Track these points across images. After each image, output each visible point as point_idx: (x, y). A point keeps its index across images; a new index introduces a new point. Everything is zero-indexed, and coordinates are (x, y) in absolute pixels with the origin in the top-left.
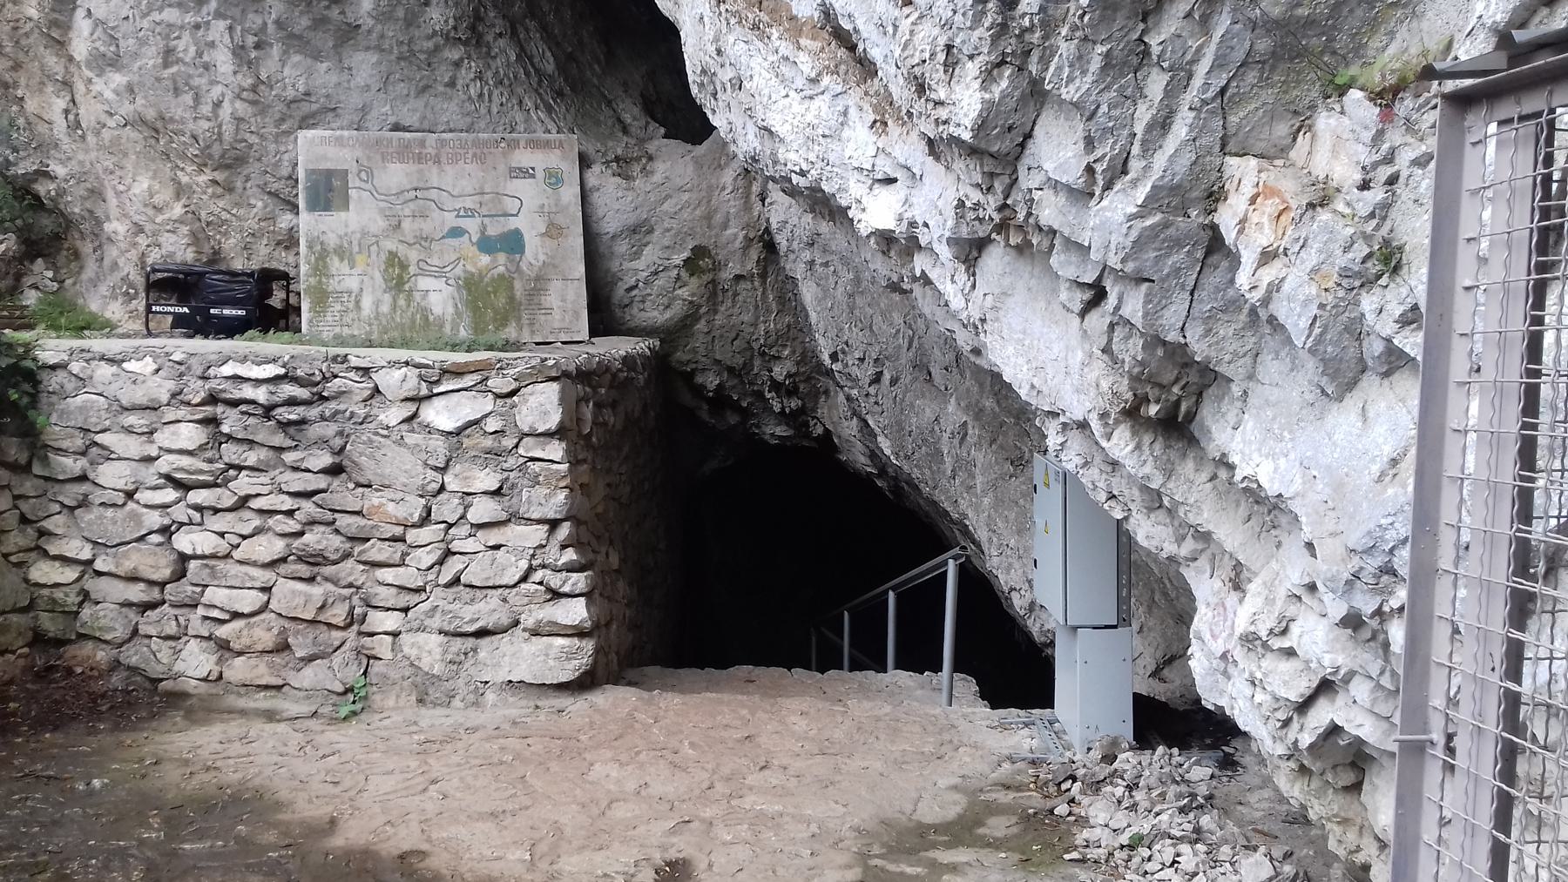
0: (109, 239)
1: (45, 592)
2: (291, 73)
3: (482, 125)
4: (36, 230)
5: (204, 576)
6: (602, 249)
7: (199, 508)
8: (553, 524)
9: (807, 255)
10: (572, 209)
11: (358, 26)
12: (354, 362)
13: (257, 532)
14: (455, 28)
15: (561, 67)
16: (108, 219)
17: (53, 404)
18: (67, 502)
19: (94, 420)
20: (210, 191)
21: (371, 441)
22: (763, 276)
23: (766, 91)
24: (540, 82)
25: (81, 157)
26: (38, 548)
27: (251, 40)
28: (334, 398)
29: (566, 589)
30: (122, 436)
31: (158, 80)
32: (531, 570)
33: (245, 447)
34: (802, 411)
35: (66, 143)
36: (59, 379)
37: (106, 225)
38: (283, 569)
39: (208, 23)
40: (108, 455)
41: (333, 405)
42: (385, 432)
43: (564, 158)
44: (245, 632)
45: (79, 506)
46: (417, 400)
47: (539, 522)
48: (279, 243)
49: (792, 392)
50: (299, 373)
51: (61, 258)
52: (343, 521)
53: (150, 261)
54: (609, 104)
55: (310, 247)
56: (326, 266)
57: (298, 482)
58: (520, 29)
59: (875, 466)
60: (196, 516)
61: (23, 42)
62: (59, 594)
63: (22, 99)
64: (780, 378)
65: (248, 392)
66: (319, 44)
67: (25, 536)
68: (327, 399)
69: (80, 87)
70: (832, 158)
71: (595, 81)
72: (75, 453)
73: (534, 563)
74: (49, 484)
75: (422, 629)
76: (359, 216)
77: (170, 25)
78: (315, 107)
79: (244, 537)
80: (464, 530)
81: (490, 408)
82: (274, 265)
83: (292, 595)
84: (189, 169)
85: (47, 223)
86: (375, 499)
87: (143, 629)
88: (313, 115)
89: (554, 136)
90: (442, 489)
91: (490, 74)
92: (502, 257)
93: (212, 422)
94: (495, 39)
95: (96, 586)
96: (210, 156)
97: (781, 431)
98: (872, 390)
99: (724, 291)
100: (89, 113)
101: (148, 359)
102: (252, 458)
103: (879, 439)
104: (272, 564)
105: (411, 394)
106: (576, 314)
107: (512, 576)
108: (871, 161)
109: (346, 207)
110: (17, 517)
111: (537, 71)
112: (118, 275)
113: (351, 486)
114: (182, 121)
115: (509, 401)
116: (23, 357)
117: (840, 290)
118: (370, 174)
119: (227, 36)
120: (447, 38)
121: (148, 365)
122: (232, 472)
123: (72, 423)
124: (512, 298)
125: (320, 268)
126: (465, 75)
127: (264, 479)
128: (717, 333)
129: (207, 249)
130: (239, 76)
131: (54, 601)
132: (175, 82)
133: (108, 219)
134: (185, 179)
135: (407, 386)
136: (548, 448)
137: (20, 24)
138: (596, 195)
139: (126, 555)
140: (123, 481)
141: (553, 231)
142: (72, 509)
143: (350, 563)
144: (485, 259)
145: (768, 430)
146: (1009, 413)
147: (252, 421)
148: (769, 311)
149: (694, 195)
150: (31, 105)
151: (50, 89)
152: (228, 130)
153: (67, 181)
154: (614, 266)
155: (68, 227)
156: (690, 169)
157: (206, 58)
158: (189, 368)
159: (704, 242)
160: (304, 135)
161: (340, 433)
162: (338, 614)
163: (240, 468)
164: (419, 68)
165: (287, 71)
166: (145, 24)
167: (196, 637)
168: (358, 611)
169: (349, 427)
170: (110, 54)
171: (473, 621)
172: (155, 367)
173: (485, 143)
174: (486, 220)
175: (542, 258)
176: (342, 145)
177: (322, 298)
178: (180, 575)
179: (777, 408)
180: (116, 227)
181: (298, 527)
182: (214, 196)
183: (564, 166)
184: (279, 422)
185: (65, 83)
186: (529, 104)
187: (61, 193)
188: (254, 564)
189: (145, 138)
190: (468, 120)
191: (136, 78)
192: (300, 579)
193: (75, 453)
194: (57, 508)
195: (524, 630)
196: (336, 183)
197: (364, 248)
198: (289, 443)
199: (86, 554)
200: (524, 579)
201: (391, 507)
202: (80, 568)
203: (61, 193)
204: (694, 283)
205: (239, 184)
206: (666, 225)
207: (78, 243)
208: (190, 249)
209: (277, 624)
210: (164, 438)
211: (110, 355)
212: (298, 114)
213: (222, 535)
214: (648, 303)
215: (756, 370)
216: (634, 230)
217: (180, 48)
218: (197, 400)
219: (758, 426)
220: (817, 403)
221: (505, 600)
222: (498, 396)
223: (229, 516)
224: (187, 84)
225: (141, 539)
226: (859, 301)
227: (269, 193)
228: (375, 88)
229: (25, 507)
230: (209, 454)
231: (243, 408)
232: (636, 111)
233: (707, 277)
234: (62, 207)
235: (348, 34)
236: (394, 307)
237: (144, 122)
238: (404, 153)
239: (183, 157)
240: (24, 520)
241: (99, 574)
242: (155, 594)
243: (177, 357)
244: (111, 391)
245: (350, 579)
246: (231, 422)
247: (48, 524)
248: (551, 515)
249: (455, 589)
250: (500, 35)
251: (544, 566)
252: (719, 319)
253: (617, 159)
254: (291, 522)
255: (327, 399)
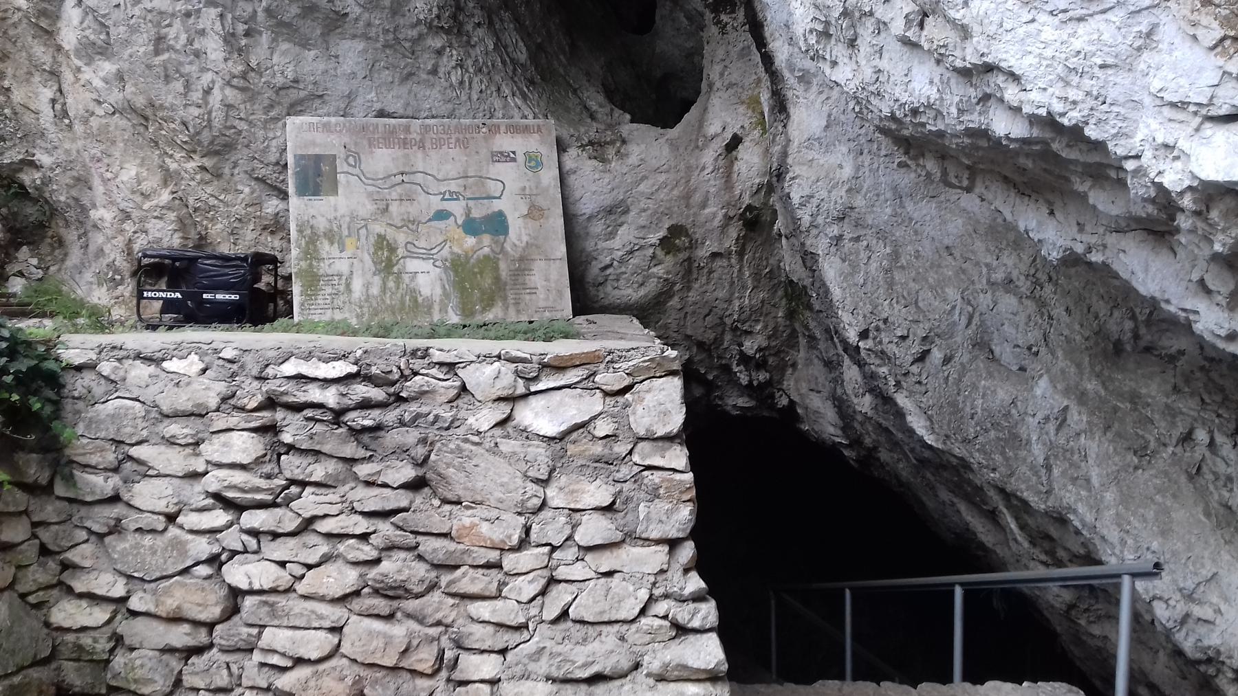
0: (95, 226)
1: (70, 638)
2: (279, 60)
3: (463, 111)
4: (20, 218)
5: (263, 615)
6: (577, 230)
7: (254, 533)
8: (673, 544)
9: (834, 230)
10: (551, 191)
11: (346, 14)
12: (437, 356)
13: (325, 559)
14: (438, 17)
15: (533, 57)
16: (94, 206)
17: (78, 412)
18: (96, 528)
19: (128, 430)
20: (198, 177)
21: (458, 448)
22: (741, 254)
23: (995, 18)
24: (515, 69)
25: (67, 146)
26: (60, 583)
27: (241, 28)
28: (414, 399)
29: (696, 624)
30: (163, 448)
31: (149, 67)
32: (651, 599)
33: (310, 459)
34: (769, 383)
35: (53, 133)
36: (86, 382)
37: (92, 213)
38: (356, 604)
39: (199, 11)
40: (145, 471)
41: (413, 407)
42: (476, 439)
43: (542, 142)
44: (312, 683)
45: (110, 533)
46: (512, 399)
47: (658, 542)
48: (265, 228)
49: (761, 365)
50: (374, 370)
51: (45, 248)
52: (429, 545)
53: (136, 247)
54: (575, 91)
55: (300, 231)
56: (316, 250)
57: (373, 500)
58: (496, 20)
59: (847, 437)
60: (252, 543)
61: (11, 32)
62: (86, 640)
63: (8, 89)
64: (751, 352)
65: (315, 394)
66: (307, 31)
67: (45, 570)
68: (405, 400)
69: (68, 76)
70: (1112, 94)
71: (561, 71)
72: (106, 470)
73: (657, 592)
74: (75, 507)
75: (525, 676)
76: (346, 201)
77: (161, 13)
78: (302, 94)
79: (309, 567)
80: (570, 553)
81: (599, 408)
82: (261, 250)
83: (368, 636)
84: (178, 156)
85: (31, 212)
86: (465, 518)
87: (188, 680)
88: (300, 102)
89: (530, 121)
90: (544, 505)
91: (470, 62)
92: (487, 239)
93: (270, 429)
94: (474, 29)
95: (133, 630)
96: (199, 143)
97: (742, 402)
98: (915, 369)
99: (700, 268)
100: (76, 101)
101: (194, 358)
102: (319, 472)
103: (909, 418)
104: (343, 599)
105: (505, 393)
106: (560, 293)
107: (630, 609)
108: (1208, 92)
109: (334, 191)
110: (36, 550)
111: (512, 60)
112: (105, 261)
113: (436, 502)
114: (172, 108)
115: (621, 399)
116: (43, 358)
117: (874, 266)
118: (358, 160)
119: (218, 24)
120: (430, 27)
121: (192, 365)
122: (294, 490)
123: (103, 434)
124: (497, 279)
125: (310, 252)
126: (447, 63)
127: (333, 496)
128: (689, 309)
129: (193, 235)
130: (230, 63)
131: (80, 648)
132: (166, 69)
133: (94, 206)
134: (173, 166)
135: (500, 384)
136: (667, 454)
137: (9, 14)
138: (573, 177)
139: (167, 592)
140: (163, 503)
141: (535, 212)
142: (101, 536)
143: (436, 596)
144: (471, 241)
145: (731, 402)
146: (1121, 396)
147: (319, 428)
148: (744, 287)
149: (672, 176)
150: (18, 96)
151: (37, 78)
152: (218, 117)
153: (52, 170)
154: (589, 245)
155: (52, 215)
156: (666, 151)
157: (196, 45)
158: (242, 367)
159: (682, 221)
160: (293, 122)
161: (423, 441)
162: (424, 659)
163: (303, 484)
164: (404, 56)
165: (276, 59)
166: (137, 11)
167: (252, 688)
168: (449, 655)
169: (432, 433)
170: (100, 43)
171: (586, 665)
172: (202, 366)
173: (467, 128)
174: (471, 203)
175: (525, 238)
176: (330, 131)
177: (313, 281)
178: (232, 611)
179: (744, 380)
180: (103, 214)
181: (374, 554)
182: (202, 182)
183: (544, 150)
184: (351, 429)
185: (52, 73)
186: (506, 91)
187: (47, 181)
188: (322, 599)
189: (134, 126)
190: (450, 106)
191: (126, 66)
192: (378, 616)
193: (106, 470)
194: (83, 535)
195: (648, 675)
196: (325, 168)
197: (353, 232)
198: (362, 453)
199: (119, 591)
200: (643, 612)
201: (485, 528)
202: (112, 607)
203: (47, 181)
204: (669, 261)
205: (227, 171)
206: (642, 205)
207: (63, 231)
208: (176, 235)
209: (352, 672)
210: (213, 450)
211: (147, 352)
212: (286, 101)
213: (282, 564)
214: (622, 282)
215: (726, 344)
216: (610, 211)
217: (171, 36)
218: (253, 404)
219: (721, 398)
220: (783, 375)
221: (622, 639)
222: (606, 394)
223: (292, 542)
224: (177, 71)
225: (186, 571)
226: (898, 276)
227: (257, 179)
228: (360, 75)
229: (45, 535)
230: (267, 468)
231: (309, 413)
232: (601, 98)
233: (682, 256)
234: (47, 195)
235: (336, 22)
236: (384, 289)
237: (134, 110)
238: (389, 139)
239: (172, 143)
240: (44, 551)
241: (134, 614)
242: (202, 637)
243: (228, 353)
244: (147, 395)
245: (439, 616)
246: (293, 430)
247: (73, 556)
248: (673, 534)
249: (563, 626)
250: (479, 25)
251: (666, 596)
252: (693, 296)
253: (591, 143)
254: (367, 548)
255: (405, 400)
